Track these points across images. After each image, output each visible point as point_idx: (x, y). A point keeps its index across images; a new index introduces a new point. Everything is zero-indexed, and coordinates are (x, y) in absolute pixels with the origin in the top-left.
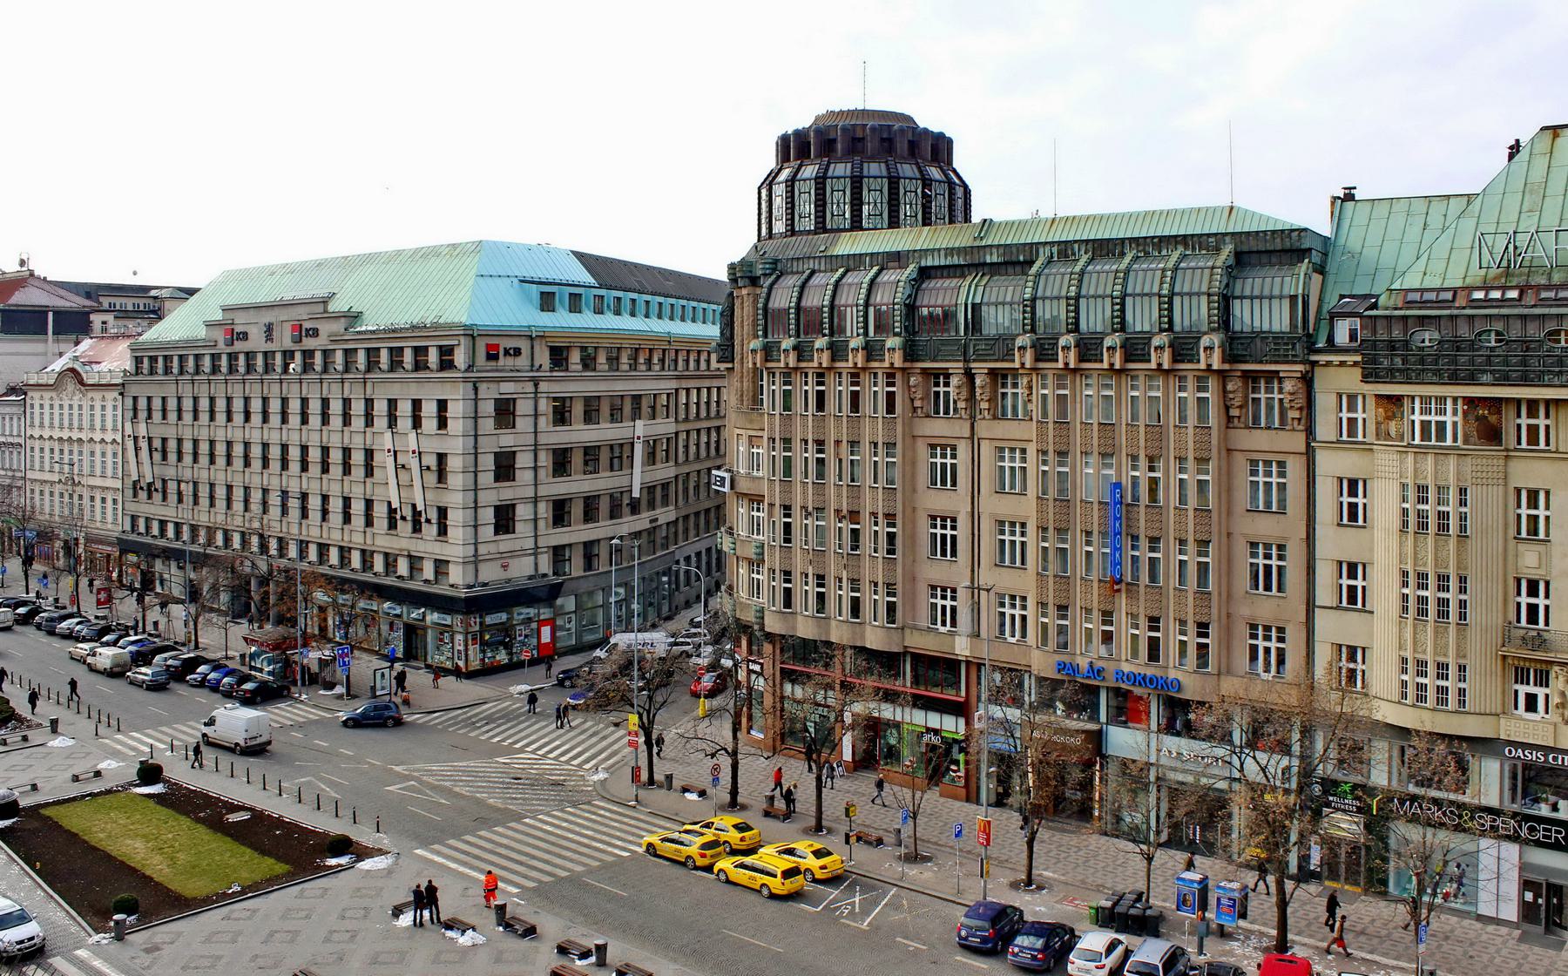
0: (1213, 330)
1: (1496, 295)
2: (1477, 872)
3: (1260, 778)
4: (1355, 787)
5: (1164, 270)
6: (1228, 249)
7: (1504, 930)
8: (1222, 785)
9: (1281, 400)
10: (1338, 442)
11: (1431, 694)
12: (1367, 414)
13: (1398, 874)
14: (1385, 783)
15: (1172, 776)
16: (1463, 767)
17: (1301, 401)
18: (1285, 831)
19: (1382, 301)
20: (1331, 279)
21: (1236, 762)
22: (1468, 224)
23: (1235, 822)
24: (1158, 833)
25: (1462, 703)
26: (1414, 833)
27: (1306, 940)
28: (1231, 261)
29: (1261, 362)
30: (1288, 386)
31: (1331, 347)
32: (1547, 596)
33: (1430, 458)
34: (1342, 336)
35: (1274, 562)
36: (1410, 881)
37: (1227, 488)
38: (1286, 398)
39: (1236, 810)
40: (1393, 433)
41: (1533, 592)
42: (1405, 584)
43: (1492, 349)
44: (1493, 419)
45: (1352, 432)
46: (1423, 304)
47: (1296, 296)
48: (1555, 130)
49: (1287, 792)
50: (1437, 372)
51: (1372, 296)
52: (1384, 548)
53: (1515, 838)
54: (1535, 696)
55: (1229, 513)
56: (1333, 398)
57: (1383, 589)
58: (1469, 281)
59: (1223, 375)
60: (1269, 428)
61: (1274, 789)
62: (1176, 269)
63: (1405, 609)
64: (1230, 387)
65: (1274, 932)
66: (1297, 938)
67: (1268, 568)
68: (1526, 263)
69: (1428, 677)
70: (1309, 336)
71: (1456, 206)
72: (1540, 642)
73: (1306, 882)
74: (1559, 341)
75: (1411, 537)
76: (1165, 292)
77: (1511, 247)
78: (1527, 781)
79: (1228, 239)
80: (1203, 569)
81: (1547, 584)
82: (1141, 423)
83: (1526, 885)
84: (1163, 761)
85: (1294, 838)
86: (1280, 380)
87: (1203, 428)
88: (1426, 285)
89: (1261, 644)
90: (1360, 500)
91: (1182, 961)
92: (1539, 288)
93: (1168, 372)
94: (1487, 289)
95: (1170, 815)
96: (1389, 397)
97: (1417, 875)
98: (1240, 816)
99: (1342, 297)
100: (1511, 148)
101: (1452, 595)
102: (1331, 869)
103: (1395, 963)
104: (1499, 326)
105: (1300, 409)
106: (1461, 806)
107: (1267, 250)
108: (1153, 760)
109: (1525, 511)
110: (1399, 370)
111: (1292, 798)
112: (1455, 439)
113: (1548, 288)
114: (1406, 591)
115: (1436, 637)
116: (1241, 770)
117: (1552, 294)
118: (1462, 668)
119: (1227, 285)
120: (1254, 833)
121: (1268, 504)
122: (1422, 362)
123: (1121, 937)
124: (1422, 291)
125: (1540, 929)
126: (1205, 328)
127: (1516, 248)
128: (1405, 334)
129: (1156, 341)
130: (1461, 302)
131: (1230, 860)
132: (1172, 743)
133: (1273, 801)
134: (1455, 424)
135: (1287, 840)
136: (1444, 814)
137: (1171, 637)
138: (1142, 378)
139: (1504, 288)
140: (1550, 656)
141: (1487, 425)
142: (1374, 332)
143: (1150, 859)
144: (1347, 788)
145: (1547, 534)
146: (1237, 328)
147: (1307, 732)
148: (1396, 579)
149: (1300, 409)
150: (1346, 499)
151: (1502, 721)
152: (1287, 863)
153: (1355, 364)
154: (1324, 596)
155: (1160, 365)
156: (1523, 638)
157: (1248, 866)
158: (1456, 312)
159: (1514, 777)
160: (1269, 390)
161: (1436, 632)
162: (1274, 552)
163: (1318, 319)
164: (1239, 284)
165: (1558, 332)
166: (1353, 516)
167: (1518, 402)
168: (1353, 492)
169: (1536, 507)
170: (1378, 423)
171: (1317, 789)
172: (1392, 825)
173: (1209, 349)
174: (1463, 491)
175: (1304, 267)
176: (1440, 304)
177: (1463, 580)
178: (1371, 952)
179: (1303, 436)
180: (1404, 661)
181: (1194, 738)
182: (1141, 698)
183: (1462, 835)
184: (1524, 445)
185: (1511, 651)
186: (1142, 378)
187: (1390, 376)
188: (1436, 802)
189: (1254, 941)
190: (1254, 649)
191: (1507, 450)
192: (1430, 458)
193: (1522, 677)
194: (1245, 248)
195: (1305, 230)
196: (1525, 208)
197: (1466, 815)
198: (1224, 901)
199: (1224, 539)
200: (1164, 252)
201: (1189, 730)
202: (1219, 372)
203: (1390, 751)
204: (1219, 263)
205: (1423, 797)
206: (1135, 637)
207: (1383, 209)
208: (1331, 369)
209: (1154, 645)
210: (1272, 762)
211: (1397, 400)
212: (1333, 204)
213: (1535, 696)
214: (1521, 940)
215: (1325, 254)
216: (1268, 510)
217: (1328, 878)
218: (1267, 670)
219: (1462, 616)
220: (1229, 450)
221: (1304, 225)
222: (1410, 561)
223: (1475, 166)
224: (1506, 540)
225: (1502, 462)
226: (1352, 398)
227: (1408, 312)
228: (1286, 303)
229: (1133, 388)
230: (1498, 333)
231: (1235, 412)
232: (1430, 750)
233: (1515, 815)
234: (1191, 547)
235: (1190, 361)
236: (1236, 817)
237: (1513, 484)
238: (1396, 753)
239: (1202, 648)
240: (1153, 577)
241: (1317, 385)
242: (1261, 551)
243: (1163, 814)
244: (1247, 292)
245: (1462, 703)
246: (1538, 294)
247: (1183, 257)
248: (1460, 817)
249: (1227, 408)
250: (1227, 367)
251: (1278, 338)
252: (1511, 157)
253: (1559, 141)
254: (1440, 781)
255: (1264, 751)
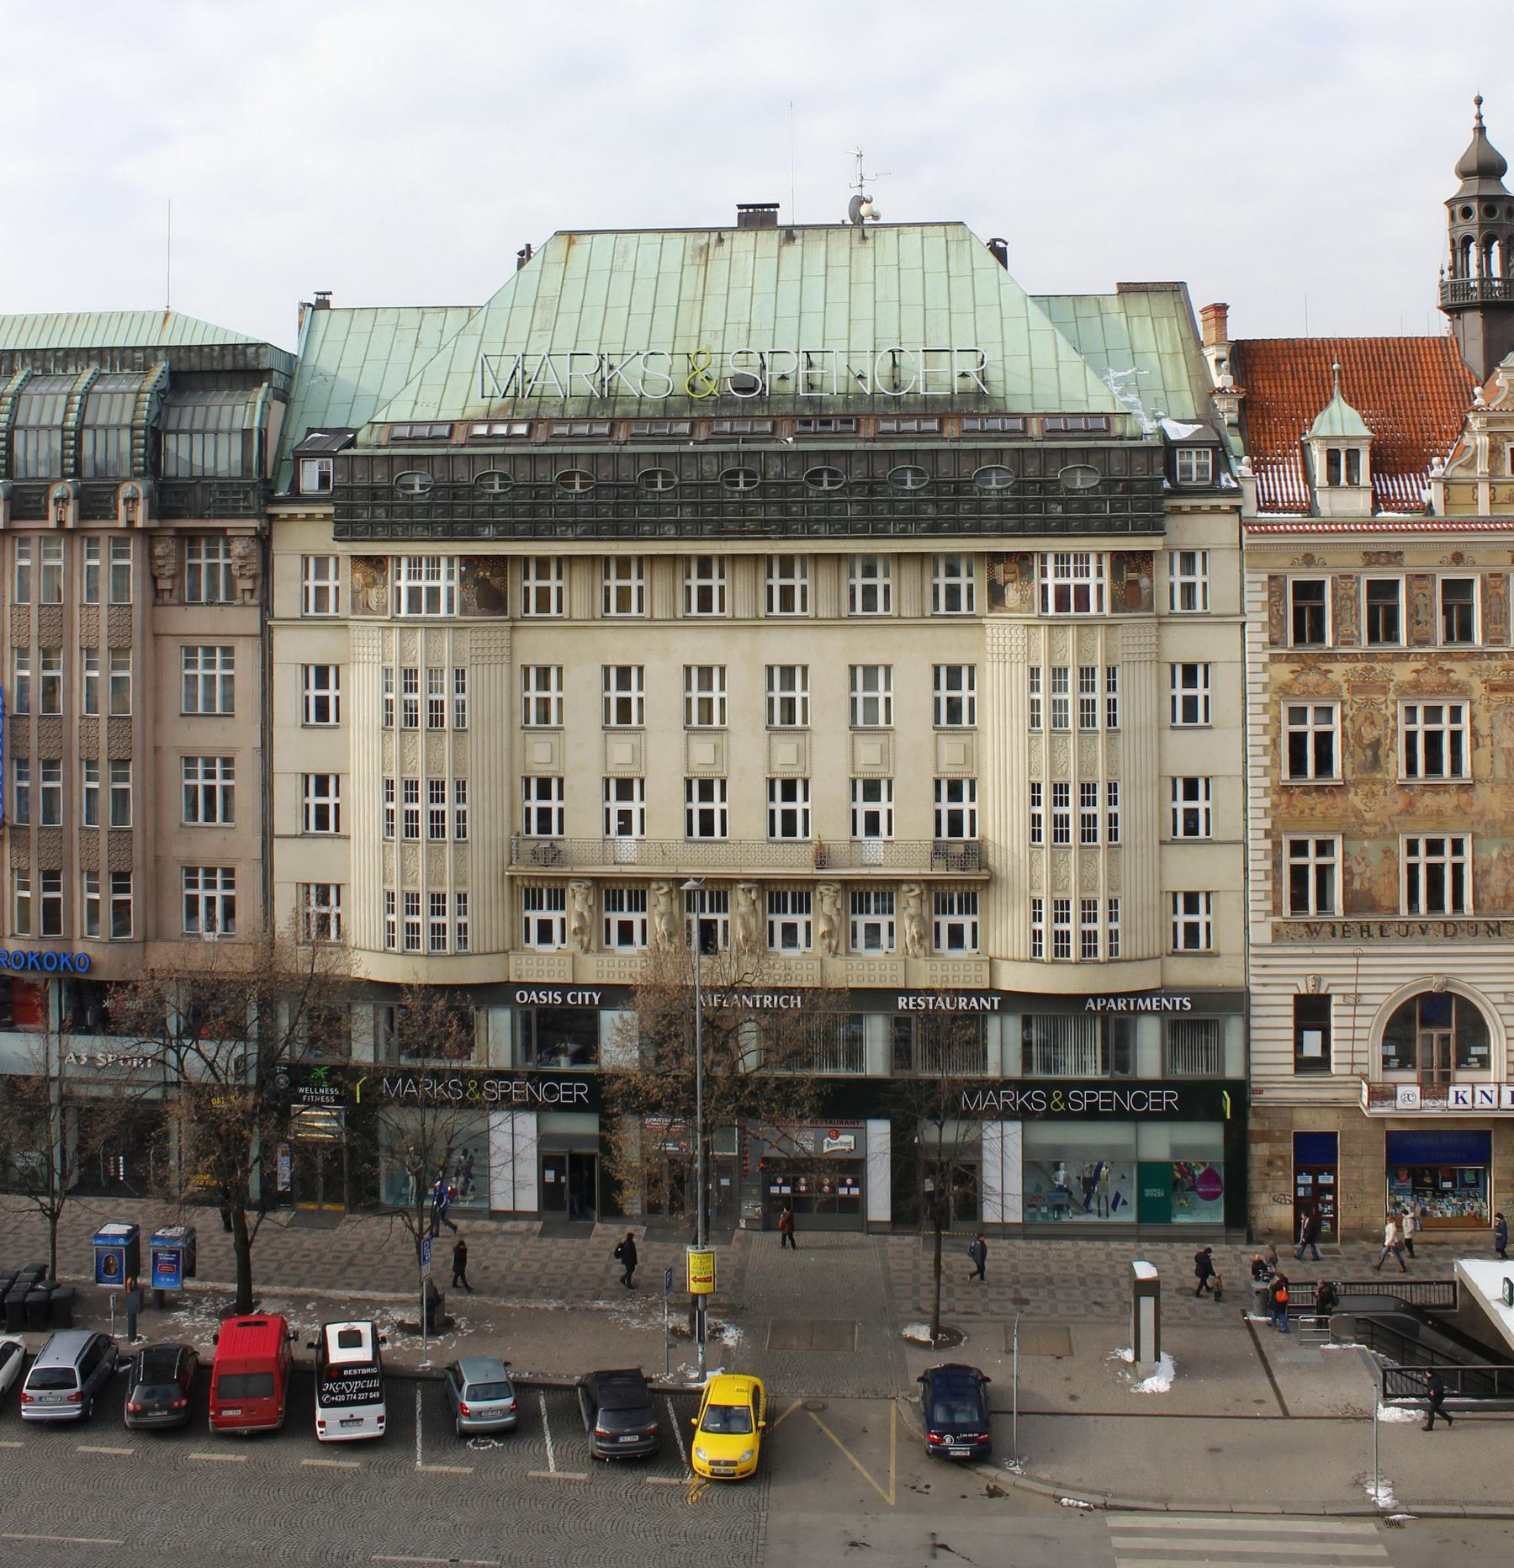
0: (137, 475)
1: (501, 429)
2: (488, 1157)
3: (207, 1077)
4: (333, 1070)
5: (70, 395)
6: (160, 368)
7: (523, 1225)
8: (155, 1094)
9: (228, 566)
10: (303, 618)
11: (424, 936)
12: (340, 581)
13: (391, 1177)
14: (371, 1059)
15: (82, 1091)
16: (467, 1025)
17: (255, 567)
18: (243, 1143)
19: (362, 437)
20: (297, 408)
21: (172, 1057)
22: (470, 343)
23: (173, 1144)
24: (63, 1177)
25: (463, 941)
26: (410, 1120)
27: (277, 1289)
28: (164, 384)
29: (202, 517)
30: (238, 548)
31: (296, 496)
32: (561, 797)
33: (420, 635)
34: (309, 480)
35: (219, 782)
36: (407, 1183)
37: (153, 687)
38: (236, 563)
39: (173, 1126)
40: (373, 604)
41: (544, 793)
42: (390, 797)
43: (496, 496)
44: (496, 582)
45: (321, 604)
46: (413, 440)
47: (251, 430)
48: (571, 236)
49: (244, 1090)
50: (426, 526)
51: (349, 430)
52: (364, 753)
53: (530, 1106)
54: (630, 924)
55: (157, 720)
56: (296, 564)
57: (362, 805)
58: (470, 413)
59: (149, 535)
60: (210, 604)
61: (225, 1090)
62: (87, 393)
63: (390, 829)
64: (159, 551)
65: (234, 1287)
66: (265, 1289)
67: (209, 791)
68: (536, 392)
69: (421, 916)
70: (266, 481)
71: (454, 320)
72: (554, 855)
73: (274, 1209)
74: (573, 486)
75: (396, 736)
76: (71, 424)
77: (519, 373)
78: (543, 1027)
79: (161, 354)
80: (121, 797)
81: (561, 781)
82: (33, 603)
83: (545, 1162)
84: (70, 1072)
85: (254, 1152)
86: (228, 541)
87: (120, 605)
88: (417, 417)
89: (202, 893)
90: (331, 693)
91: (108, 1354)
92: (551, 421)
93: (72, 532)
94: (490, 421)
95: (80, 1149)
96: (368, 559)
97: (416, 1174)
98: (180, 1133)
99: (311, 431)
100: (521, 253)
101: (448, 807)
102: (303, 1187)
103: (391, 1296)
104: (503, 468)
105: (254, 577)
106: (465, 1075)
107: (206, 371)
108: (54, 1072)
109: (534, 694)
110: (382, 524)
111: (251, 1097)
112: (1100, 608)
113: (562, 421)
114: (391, 806)
115: (1082, 866)
116: (180, 1070)
117: (565, 430)
118: (462, 898)
119: (159, 415)
120: (201, 1154)
121: (210, 701)
122: (410, 514)
123: (16, 1339)
124: (412, 424)
125: (566, 1214)
126: (126, 473)
127: (524, 373)
128: (390, 479)
129: (56, 491)
130: (459, 437)
131: (169, 1198)
132: (82, 1045)
133: (225, 1106)
134: (450, 590)
135: (246, 1156)
136: (446, 1088)
137: (78, 896)
138: (35, 541)
139: (510, 422)
140: (565, 871)
141: (489, 589)
142: (352, 476)
143: (54, 1216)
144: (321, 1073)
145: (560, 720)
146: (171, 471)
147: (267, 1007)
148: (379, 790)
149: (254, 577)
150: (313, 693)
151: (512, 959)
152: (247, 1188)
153: (326, 517)
154: (287, 818)
155: (61, 523)
156: (534, 852)
157: (196, 1201)
158: (453, 451)
159: (527, 1027)
160: (212, 553)
161: (429, 854)
162: (218, 768)
163: (279, 460)
164: (174, 414)
165: (571, 475)
166: (322, 714)
167: (526, 559)
168: (322, 682)
169: (547, 688)
170: (355, 593)
171: (283, 1081)
172: (381, 1114)
173: (132, 500)
174: (460, 674)
175: (260, 393)
176: (434, 440)
177: (461, 785)
178: (362, 1289)
179: (256, 612)
180: (390, 896)
181: (113, 1034)
182: (31, 987)
183: (469, 1112)
184: (533, 612)
185: (520, 869)
186: (35, 541)
187: (370, 532)
188: (436, 1074)
189: (207, 1305)
190: (193, 901)
191: (513, 620)
192: (420, 635)
193: (533, 902)
194: (184, 367)
195: (265, 345)
196: (536, 326)
197: (472, 1085)
198: (163, 1257)
199: (150, 755)
200: (71, 370)
201: (105, 1024)
202: (144, 530)
203: (376, 1014)
204: (148, 386)
205: (419, 1071)
206: (24, 902)
207: (365, 321)
208: (295, 526)
209: (51, 910)
210: (223, 1052)
211: (377, 563)
212: (301, 312)
213: (630, 924)
214: (543, 1234)
215: (290, 377)
216: (210, 714)
217: (304, 1199)
218: (211, 927)
219: (461, 832)
220: (156, 635)
221: (262, 340)
222: (395, 767)
223: (482, 274)
224: (511, 732)
225: (506, 635)
226: (321, 561)
227: (395, 451)
228: (237, 442)
229: (22, 555)
230: (503, 477)
231: (165, 584)
232: (427, 1009)
233: (531, 1076)
234: (104, 770)
235: (104, 517)
236: (174, 1137)
237: (519, 662)
238: (382, 1018)
239: (121, 909)
240: (49, 816)
241: (277, 546)
242: (200, 768)
243: (71, 1148)
244: (185, 425)
245: (463, 941)
246: (549, 429)
247: (98, 378)
248: (465, 1089)
249: (155, 579)
250: (155, 524)
251: (225, 486)
252: (521, 264)
253: (575, 249)
254: (440, 1047)
255: (211, 1039)
